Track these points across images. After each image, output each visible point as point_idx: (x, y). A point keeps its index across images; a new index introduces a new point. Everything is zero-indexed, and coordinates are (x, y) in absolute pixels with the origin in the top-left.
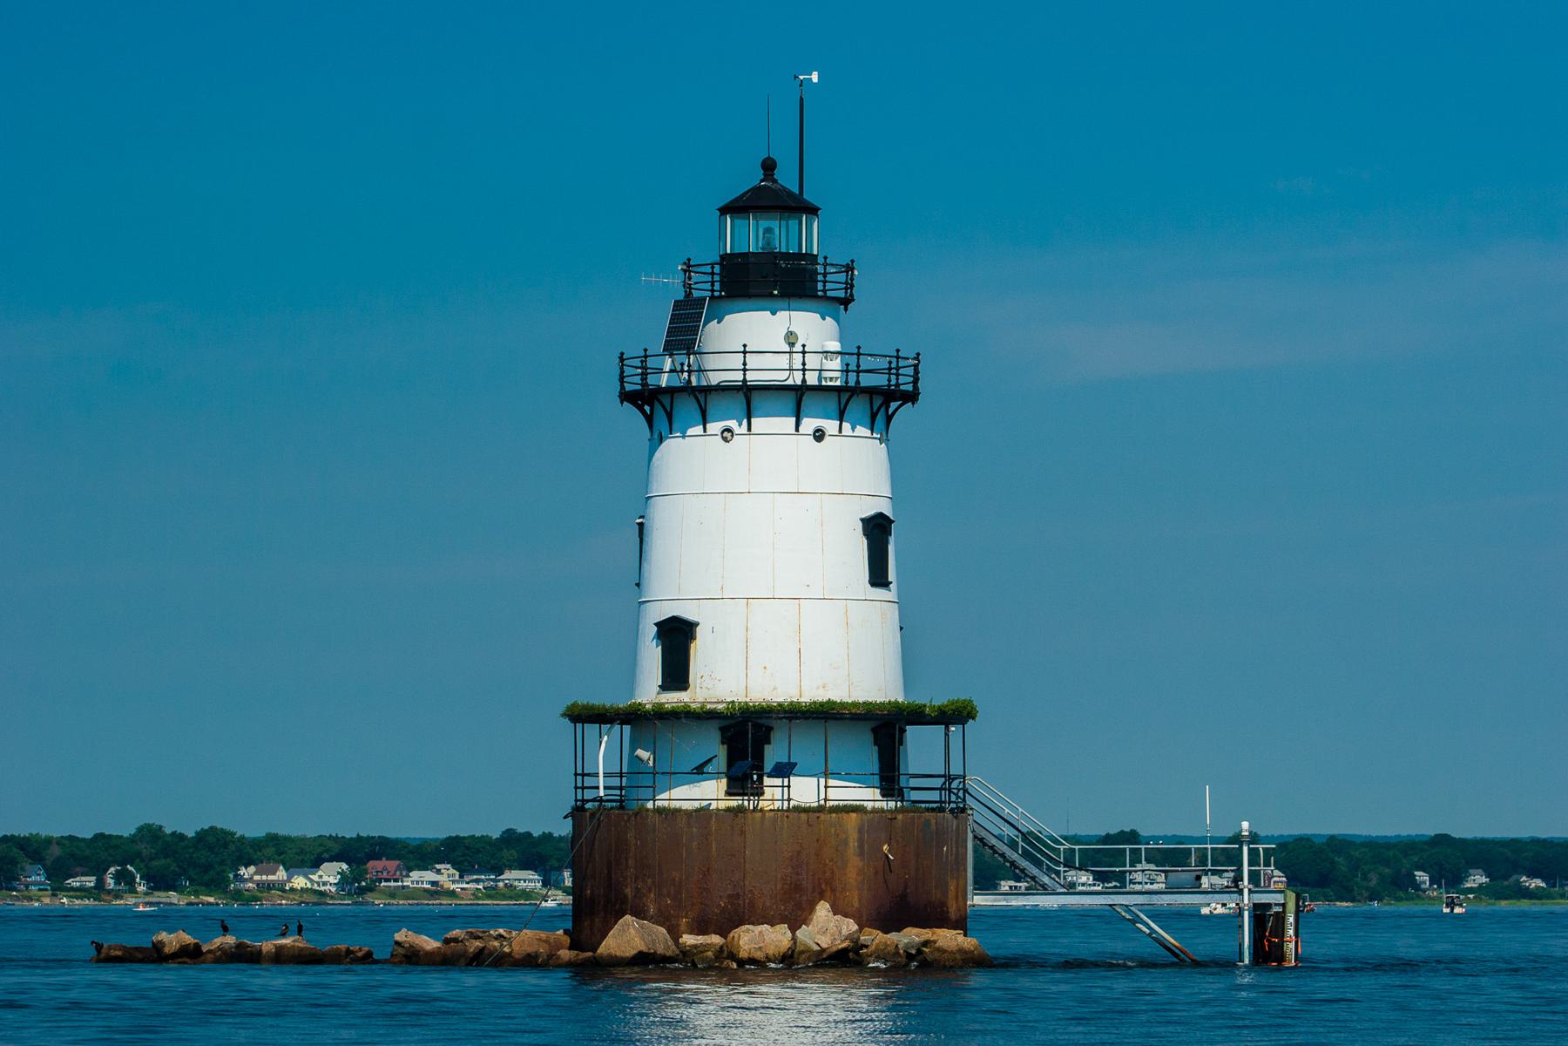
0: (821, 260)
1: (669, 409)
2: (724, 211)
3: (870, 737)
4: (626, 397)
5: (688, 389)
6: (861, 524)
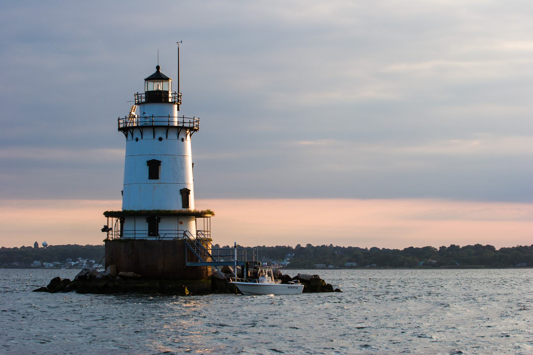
1: (132, 132)
3: (146, 221)
4: (120, 129)
6: (147, 162)
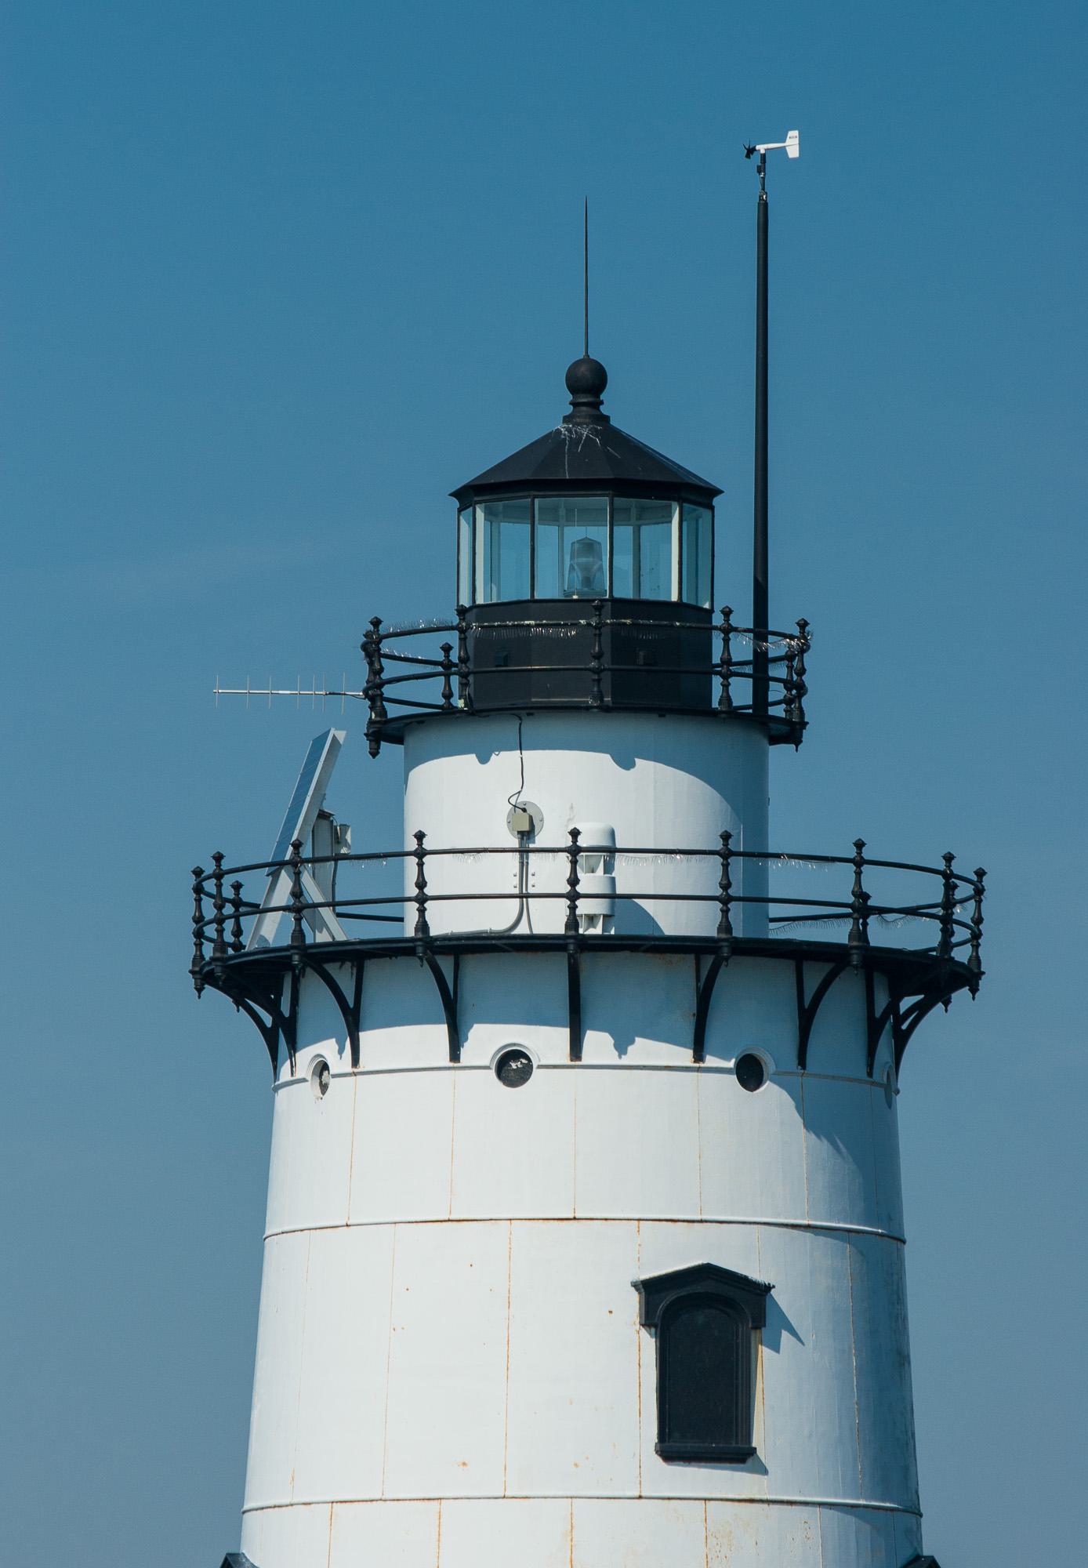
0: (718, 620)
2: (468, 495)
5: (321, 958)
